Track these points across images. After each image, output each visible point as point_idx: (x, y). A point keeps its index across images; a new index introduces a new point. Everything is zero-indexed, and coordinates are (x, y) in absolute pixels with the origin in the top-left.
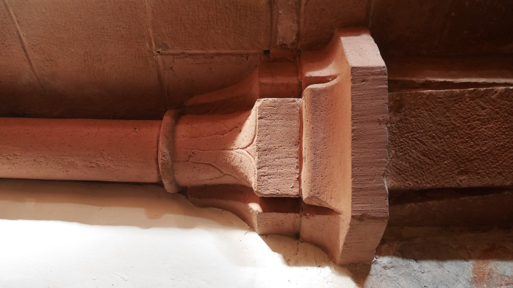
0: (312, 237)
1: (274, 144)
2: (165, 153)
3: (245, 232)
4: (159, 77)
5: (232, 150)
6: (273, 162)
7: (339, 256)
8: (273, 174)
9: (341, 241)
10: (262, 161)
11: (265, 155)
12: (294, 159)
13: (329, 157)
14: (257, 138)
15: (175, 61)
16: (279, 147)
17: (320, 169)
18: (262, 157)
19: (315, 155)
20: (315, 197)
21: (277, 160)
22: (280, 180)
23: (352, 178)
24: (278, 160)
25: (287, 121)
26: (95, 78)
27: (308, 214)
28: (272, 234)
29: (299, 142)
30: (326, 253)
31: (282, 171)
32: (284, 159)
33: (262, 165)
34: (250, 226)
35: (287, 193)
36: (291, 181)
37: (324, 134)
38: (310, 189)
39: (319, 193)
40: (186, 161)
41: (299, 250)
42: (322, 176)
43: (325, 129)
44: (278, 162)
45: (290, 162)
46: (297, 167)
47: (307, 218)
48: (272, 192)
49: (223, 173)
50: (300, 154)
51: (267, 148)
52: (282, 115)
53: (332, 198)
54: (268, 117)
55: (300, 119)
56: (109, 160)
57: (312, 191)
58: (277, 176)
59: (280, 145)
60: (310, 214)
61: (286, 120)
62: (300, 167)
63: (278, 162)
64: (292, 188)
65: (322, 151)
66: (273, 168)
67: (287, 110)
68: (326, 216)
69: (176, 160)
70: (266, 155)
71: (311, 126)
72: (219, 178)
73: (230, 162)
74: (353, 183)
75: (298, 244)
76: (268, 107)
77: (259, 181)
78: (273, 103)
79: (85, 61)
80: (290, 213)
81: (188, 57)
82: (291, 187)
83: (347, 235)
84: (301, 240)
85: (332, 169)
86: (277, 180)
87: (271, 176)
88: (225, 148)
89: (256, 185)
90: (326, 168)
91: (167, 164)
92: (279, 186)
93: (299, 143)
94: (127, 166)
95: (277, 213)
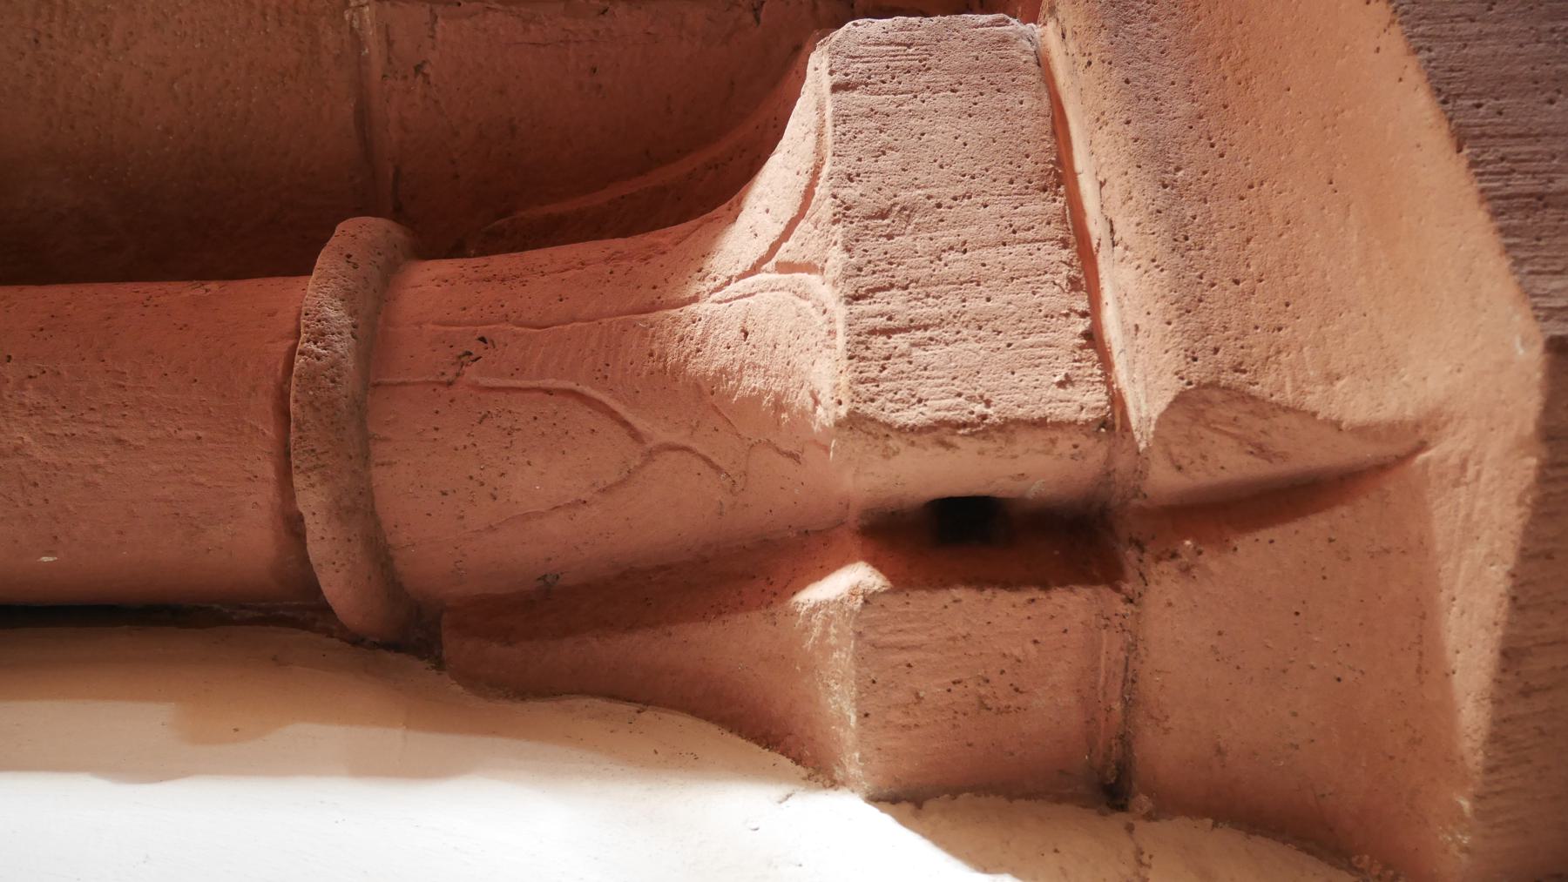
0: (1219, 751)
1: (925, 187)
2: (326, 320)
3: (777, 791)
4: (363, 116)
5: (695, 299)
6: (933, 266)
7: (1466, 804)
8: (941, 323)
9: (1458, 661)
10: (869, 262)
11: (880, 236)
12: (1047, 246)
13: (1251, 187)
14: (834, 164)
15: (439, 36)
16: (955, 199)
17: (1215, 249)
18: (868, 245)
19: (1167, 190)
20: (1227, 388)
21: (952, 256)
22: (982, 352)
23: (1459, 150)
24: (959, 256)
25: (982, 94)
26: (72, 127)
27: (1188, 543)
28: (955, 792)
29: (1057, 175)
30: (1330, 864)
31: (989, 304)
32: (993, 251)
33: (869, 281)
34: (805, 766)
35: (1036, 415)
36: (1051, 351)
37: (1193, 101)
38: (1184, 345)
39: (1241, 364)
40: (441, 383)
41: (1151, 857)
42: (1237, 282)
43: (1191, 82)
44: (962, 264)
45: (1026, 263)
46: (1074, 284)
47: (1186, 570)
48: (948, 410)
49: (642, 442)
50: (1073, 224)
51: (889, 203)
52: (949, 72)
53: (1331, 378)
54: (884, 82)
55: (1048, 87)
56: (22, 405)
57: (1195, 359)
58: (965, 332)
59: (960, 190)
60: (1198, 539)
61: (974, 92)
62: (1086, 281)
63: (958, 264)
64: (1065, 388)
65: (1205, 169)
66: (934, 293)
67: (975, 54)
68: (1312, 518)
69: (387, 380)
70: (890, 237)
71: (1117, 75)
72: (622, 483)
73: (682, 358)
74: (1480, 170)
75: (1130, 828)
76: (875, 45)
77: (864, 358)
78: (901, 30)
79: (37, 41)
80: (1062, 584)
81: (496, 10)
82: (1057, 379)
83: (1525, 555)
84: (1143, 802)
85: (1284, 237)
86: (968, 351)
87: (928, 334)
88: (653, 303)
89: (844, 380)
90: (1248, 241)
91: (333, 381)
92: (984, 383)
93: (1061, 176)
94: (119, 441)
95: (981, 589)
